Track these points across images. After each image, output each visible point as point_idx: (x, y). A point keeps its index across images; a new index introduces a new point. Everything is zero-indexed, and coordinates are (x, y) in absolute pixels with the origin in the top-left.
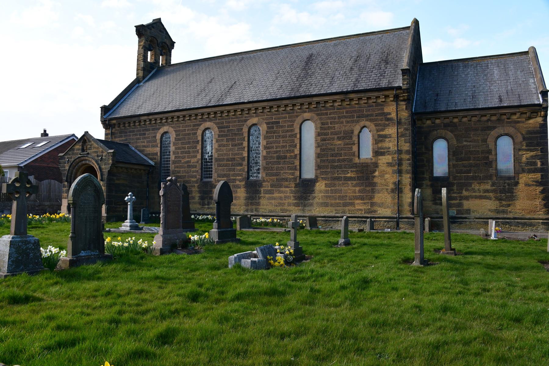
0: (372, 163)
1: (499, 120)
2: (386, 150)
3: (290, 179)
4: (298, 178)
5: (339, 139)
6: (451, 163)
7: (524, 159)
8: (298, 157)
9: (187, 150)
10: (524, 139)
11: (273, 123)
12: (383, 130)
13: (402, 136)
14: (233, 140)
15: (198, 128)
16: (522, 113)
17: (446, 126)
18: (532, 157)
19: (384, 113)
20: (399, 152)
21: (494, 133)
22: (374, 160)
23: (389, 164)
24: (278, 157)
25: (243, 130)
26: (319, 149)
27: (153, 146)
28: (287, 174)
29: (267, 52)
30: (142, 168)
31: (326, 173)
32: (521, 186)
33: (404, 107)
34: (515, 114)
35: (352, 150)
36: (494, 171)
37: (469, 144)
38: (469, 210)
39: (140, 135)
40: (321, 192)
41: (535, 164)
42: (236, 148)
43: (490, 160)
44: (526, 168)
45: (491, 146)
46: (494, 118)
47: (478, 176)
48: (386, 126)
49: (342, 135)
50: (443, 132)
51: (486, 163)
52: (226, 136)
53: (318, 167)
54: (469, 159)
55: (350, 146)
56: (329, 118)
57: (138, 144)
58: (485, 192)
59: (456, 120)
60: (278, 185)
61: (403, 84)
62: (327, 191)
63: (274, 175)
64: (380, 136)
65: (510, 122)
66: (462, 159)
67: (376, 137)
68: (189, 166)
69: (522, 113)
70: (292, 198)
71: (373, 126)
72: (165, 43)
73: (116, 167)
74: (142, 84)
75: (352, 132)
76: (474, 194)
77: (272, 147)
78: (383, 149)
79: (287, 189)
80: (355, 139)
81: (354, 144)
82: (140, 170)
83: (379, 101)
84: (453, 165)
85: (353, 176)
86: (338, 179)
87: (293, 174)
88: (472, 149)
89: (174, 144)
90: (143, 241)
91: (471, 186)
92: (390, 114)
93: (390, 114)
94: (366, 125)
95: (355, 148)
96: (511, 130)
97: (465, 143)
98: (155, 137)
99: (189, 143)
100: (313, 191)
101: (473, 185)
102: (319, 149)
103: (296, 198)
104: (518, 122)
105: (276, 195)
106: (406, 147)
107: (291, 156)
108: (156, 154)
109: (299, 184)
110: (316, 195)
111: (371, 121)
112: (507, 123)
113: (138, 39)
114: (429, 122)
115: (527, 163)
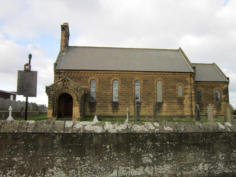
17: (201, 86)
48: (186, 85)
54: (208, 97)
64: (185, 88)
66: (206, 97)
86: (171, 102)
87: (154, 100)
111: (182, 83)
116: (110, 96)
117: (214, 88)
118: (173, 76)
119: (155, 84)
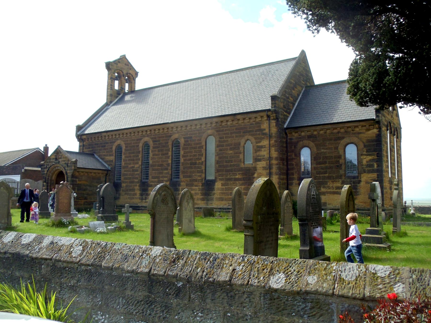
0: (253, 167)
1: (346, 132)
2: (262, 157)
3: (199, 180)
4: (204, 179)
5: (231, 149)
6: (313, 166)
7: (364, 162)
8: (204, 163)
9: (132, 158)
10: (365, 146)
12: (260, 142)
13: (273, 146)
14: (162, 150)
15: (140, 142)
16: (362, 126)
17: (309, 137)
18: (370, 160)
19: (261, 129)
21: (343, 142)
22: (253, 166)
23: (264, 168)
24: (191, 164)
25: (169, 143)
26: (218, 157)
27: (110, 155)
28: (197, 176)
29: (197, 81)
31: (222, 175)
32: (362, 184)
33: (275, 124)
34: (357, 127)
35: (239, 158)
36: (343, 172)
37: (325, 151)
38: (326, 203)
39: (102, 147)
40: (218, 189)
41: (372, 166)
42: (164, 156)
43: (341, 163)
44: (366, 169)
45: (341, 152)
46: (342, 130)
47: (332, 176)
49: (233, 146)
50: (306, 142)
51: (338, 166)
52: (158, 147)
53: (217, 171)
54: (325, 163)
55: (238, 155)
56: (225, 134)
57: (101, 154)
58: (336, 189)
61: (272, 107)
62: (222, 189)
63: (188, 177)
64: (258, 147)
65: (355, 133)
66: (320, 163)
67: (255, 147)
68: (133, 171)
69: (362, 126)
70: (200, 194)
71: (253, 140)
72: (130, 74)
73: (78, 172)
74: (110, 106)
75: (239, 144)
76: (329, 190)
77: (188, 156)
78: (260, 156)
79: (196, 188)
80: (241, 149)
81: (240, 153)
82: (99, 173)
83: (257, 120)
84: (314, 168)
85: (240, 177)
86: (230, 179)
88: (327, 155)
91: (327, 184)
92: (265, 130)
93: (265, 130)
94: (249, 138)
95: (241, 156)
96: (355, 139)
97: (322, 150)
98: (112, 148)
99: (134, 153)
100: (213, 189)
101: (328, 183)
102: (218, 157)
103: (203, 194)
104: (361, 133)
106: (275, 154)
107: (199, 162)
108: (112, 161)
109: (204, 183)
110: (215, 192)
111: (252, 135)
112: (353, 134)
113: (107, 72)
116: (137, 171)
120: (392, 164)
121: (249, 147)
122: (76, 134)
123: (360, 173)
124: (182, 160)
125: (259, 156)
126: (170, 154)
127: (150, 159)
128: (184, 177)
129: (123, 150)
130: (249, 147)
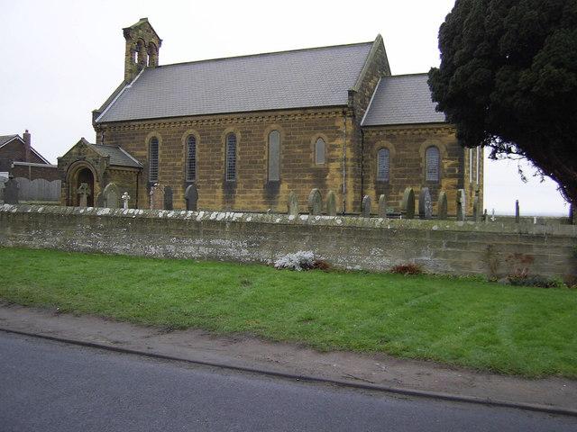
7: (446, 166)
11: (247, 132)
17: (388, 137)
18: (452, 165)
20: (345, 159)
27: (142, 150)
30: (132, 169)
48: (335, 138)
54: (405, 166)
59: (395, 133)
60: (249, 186)
64: (331, 146)
66: (399, 166)
71: (326, 138)
80: (312, 148)
86: (299, 181)
87: (262, 177)
89: (161, 156)
90: (185, 215)
95: (312, 156)
100: (278, 192)
105: (249, 195)
106: (350, 155)
111: (325, 132)
114: (374, 134)
115: (449, 170)
116: (180, 169)
117: (421, 140)
118: (304, 118)
119: (266, 139)
120: (474, 169)
121: (320, 145)
122: (93, 121)
123: (440, 178)
124: (239, 158)
125: (332, 156)
126: (223, 150)
127: (196, 155)
128: (241, 177)
129: (160, 144)
130: (320, 145)
